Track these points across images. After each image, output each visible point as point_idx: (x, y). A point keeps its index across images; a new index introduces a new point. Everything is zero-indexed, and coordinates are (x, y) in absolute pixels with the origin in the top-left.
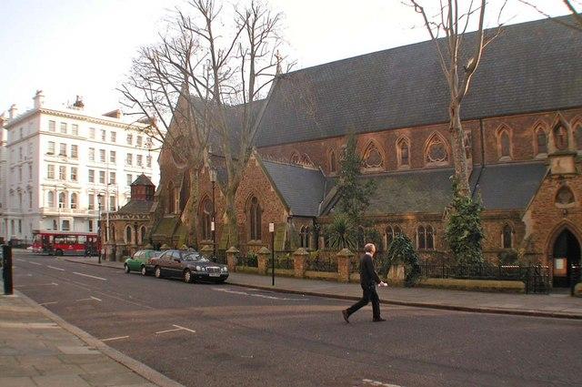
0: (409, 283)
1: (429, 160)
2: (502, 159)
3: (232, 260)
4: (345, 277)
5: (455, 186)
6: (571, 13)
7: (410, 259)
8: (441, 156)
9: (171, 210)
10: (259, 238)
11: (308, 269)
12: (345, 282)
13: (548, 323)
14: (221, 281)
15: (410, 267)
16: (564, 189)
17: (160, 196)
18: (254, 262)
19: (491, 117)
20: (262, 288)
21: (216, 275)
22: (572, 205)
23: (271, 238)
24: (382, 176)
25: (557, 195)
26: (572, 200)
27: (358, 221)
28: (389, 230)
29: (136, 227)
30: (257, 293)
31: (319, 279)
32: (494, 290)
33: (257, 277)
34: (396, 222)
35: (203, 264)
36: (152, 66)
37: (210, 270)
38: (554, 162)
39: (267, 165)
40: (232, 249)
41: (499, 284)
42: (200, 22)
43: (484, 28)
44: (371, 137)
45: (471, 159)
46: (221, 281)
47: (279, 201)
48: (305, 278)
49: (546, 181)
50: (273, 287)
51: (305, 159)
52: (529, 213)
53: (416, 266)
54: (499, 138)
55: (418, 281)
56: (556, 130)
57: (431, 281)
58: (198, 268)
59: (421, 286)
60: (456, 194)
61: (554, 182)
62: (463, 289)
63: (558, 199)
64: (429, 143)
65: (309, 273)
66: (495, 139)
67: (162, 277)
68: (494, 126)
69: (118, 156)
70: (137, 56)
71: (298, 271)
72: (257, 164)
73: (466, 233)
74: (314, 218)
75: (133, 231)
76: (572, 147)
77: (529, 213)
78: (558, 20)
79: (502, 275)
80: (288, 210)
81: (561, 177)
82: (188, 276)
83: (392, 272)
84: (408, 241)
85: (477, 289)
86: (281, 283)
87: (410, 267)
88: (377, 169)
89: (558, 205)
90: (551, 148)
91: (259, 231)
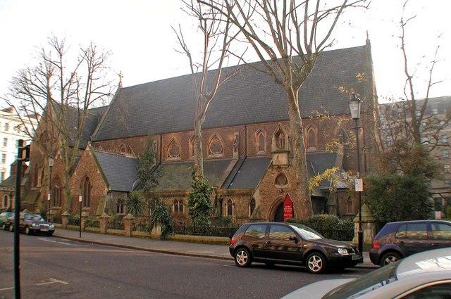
0: (164, 237)
1: (210, 153)
2: (259, 152)
3: (65, 220)
4: (129, 233)
5: (194, 173)
6: (260, 60)
7: (165, 221)
8: (219, 150)
9: (36, 184)
10: (89, 206)
11: (135, 229)
12: (128, 237)
13: (206, 261)
14: (49, 234)
15: (165, 227)
16: (281, 175)
17: (28, 174)
18: (78, 222)
19: (252, 124)
20: (72, 239)
21: (45, 230)
22: (286, 186)
23: (23, 203)
24: (178, 164)
25: (277, 179)
26: (286, 183)
27: (150, 195)
28: (176, 201)
29: (11, 196)
30: (68, 242)
31: (182, 240)
32: (212, 243)
33: (99, 236)
34: (180, 196)
35: (37, 223)
36: (24, 85)
37: (42, 227)
38: (275, 156)
39: (98, 155)
40: (65, 213)
41: (214, 238)
42: (55, 57)
43: (223, 66)
44: (174, 136)
45: (237, 153)
46: (49, 234)
47: (103, 180)
48: (106, 233)
49: (270, 170)
50: (79, 239)
51: (129, 151)
52: (258, 191)
53: (169, 226)
54: (257, 138)
55: (169, 236)
56: (277, 135)
57: (177, 236)
58: (34, 225)
59: (171, 240)
60: (194, 178)
61: (275, 171)
62: (194, 242)
63: (277, 182)
64: (211, 141)
65: (109, 231)
66: (254, 138)
67: (29, 234)
68: (254, 130)
69: (9, 142)
70: (16, 75)
71: (102, 229)
72: (90, 154)
73: (196, 204)
74: (128, 192)
75: (9, 199)
76: (287, 147)
77: (258, 191)
78: (250, 65)
79: (216, 234)
80: (108, 186)
81: (279, 167)
82: (27, 230)
83: (154, 229)
84: (164, 209)
85: (202, 242)
86: (85, 237)
87: (165, 227)
88: (176, 158)
89: (277, 186)
90: (274, 148)
91: (89, 201)
